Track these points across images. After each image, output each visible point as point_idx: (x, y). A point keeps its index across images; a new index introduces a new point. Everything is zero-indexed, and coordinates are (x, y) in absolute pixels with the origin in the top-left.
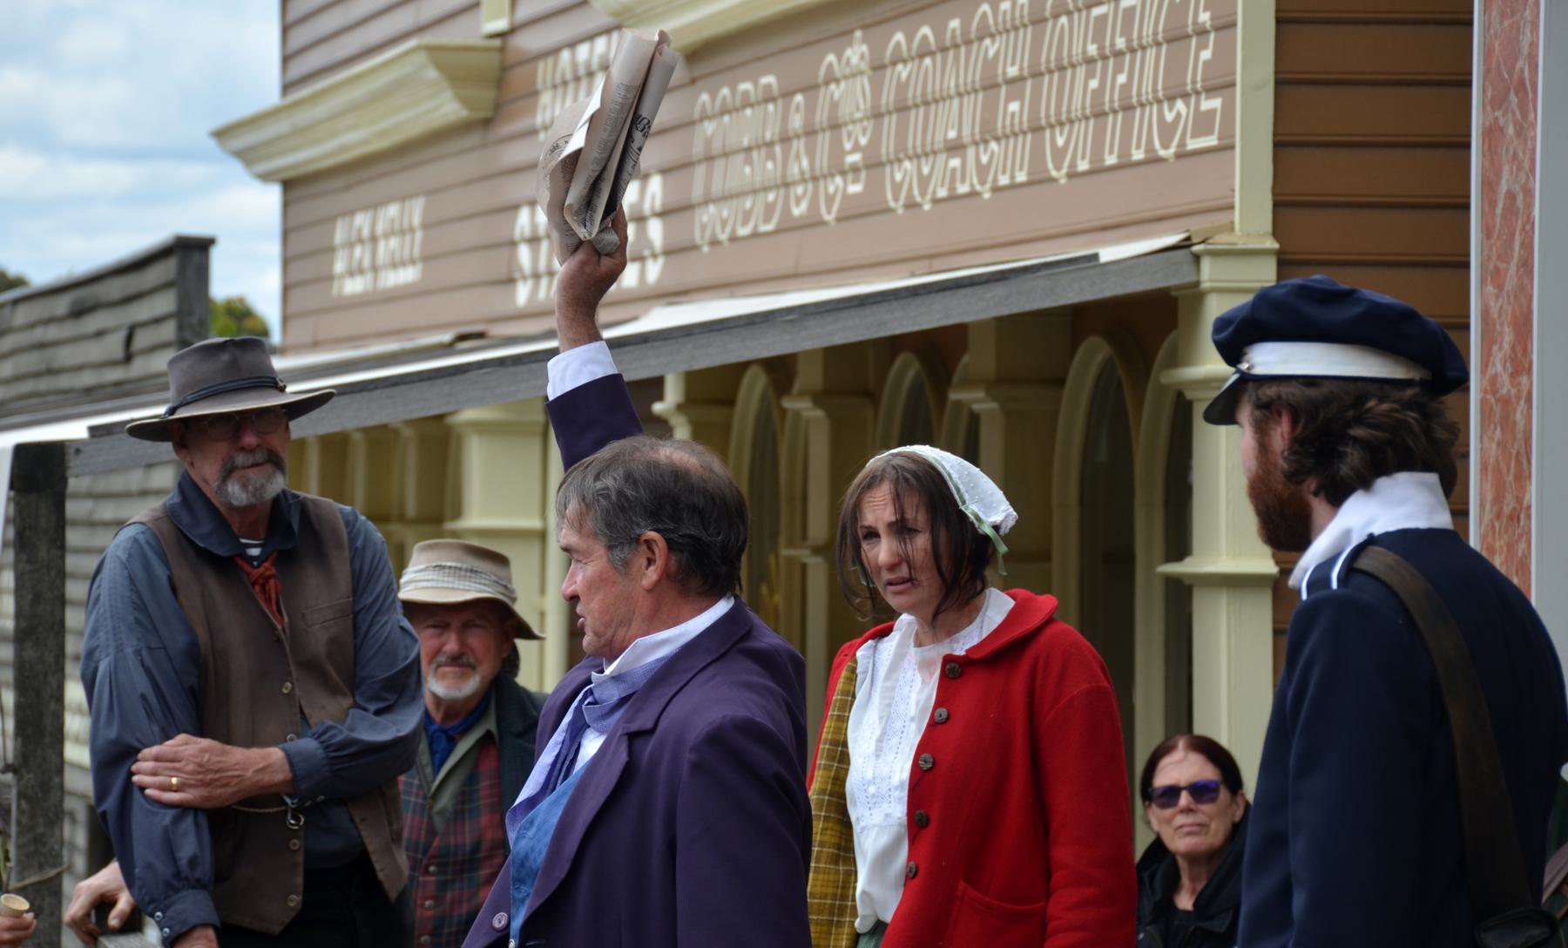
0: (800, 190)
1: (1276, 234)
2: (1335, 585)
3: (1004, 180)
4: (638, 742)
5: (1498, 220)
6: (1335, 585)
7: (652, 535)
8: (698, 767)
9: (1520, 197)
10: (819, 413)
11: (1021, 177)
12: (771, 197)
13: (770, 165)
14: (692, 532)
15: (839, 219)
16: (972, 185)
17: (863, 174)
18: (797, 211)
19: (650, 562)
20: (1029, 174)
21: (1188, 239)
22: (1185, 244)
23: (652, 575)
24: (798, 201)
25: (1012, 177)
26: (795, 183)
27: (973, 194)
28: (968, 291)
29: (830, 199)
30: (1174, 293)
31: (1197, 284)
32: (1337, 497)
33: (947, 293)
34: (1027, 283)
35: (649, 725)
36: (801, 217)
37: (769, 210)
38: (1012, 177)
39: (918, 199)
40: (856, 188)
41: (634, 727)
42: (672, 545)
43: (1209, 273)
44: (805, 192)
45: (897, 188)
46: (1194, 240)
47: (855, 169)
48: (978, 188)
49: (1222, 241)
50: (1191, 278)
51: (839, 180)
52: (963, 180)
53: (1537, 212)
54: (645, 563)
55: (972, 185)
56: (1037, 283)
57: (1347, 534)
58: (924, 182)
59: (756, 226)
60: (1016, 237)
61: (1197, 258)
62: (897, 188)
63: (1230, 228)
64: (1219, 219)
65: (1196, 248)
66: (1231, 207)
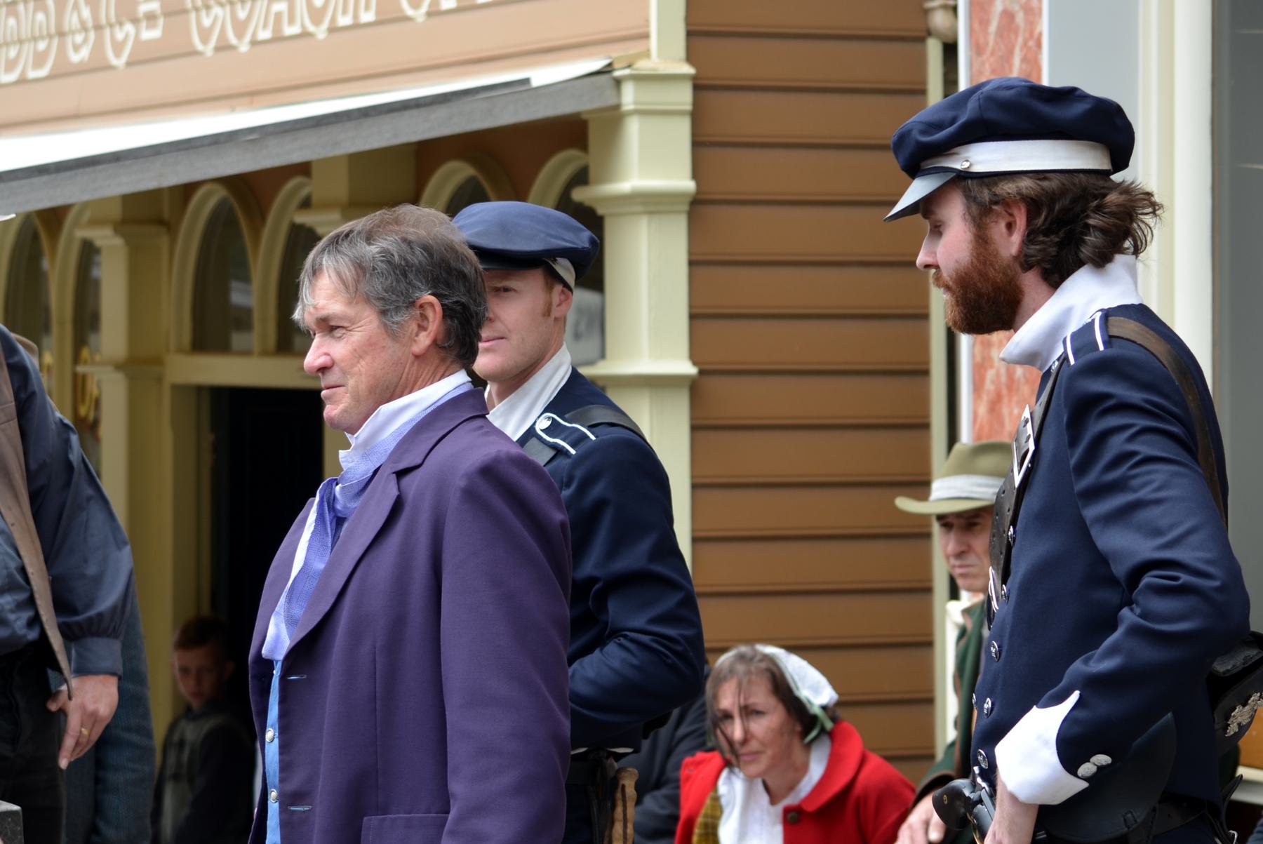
0: (79, 38)
1: (690, 59)
2: (1101, 348)
3: (344, 21)
4: (406, 480)
5: (991, 39)
6: (1101, 348)
7: (428, 298)
8: (470, 494)
9: (1020, 18)
10: (118, 241)
11: (367, 17)
12: (42, 46)
13: (40, 16)
14: (463, 300)
15: (129, 64)
16: (303, 26)
17: (161, 21)
18: (75, 58)
19: (422, 328)
20: (377, 13)
21: (610, 65)
22: (606, 70)
23: (424, 340)
24: (77, 48)
25: (356, 16)
26: (73, 32)
27: (305, 34)
28: (414, 112)
29: (118, 48)
30: (584, 117)
31: (617, 107)
32: (1055, 276)
33: (395, 114)
34: (455, 107)
35: (419, 461)
36: (81, 62)
37: (39, 60)
38: (356, 16)
39: (233, 40)
40: (151, 34)
41: (401, 466)
42: (448, 312)
43: (629, 97)
44: (85, 40)
45: (205, 35)
46: (616, 66)
47: (151, 17)
48: (311, 28)
49: (644, 66)
50: (612, 102)
51: (129, 28)
52: (291, 21)
53: (1044, 26)
54: (414, 327)
55: (303, 26)
56: (441, 112)
57: (1068, 312)
58: (240, 27)
59: (23, 72)
60: (365, 73)
61: (618, 82)
62: (205, 35)
63: (647, 54)
64: (633, 48)
65: (617, 74)
66: (646, 36)
